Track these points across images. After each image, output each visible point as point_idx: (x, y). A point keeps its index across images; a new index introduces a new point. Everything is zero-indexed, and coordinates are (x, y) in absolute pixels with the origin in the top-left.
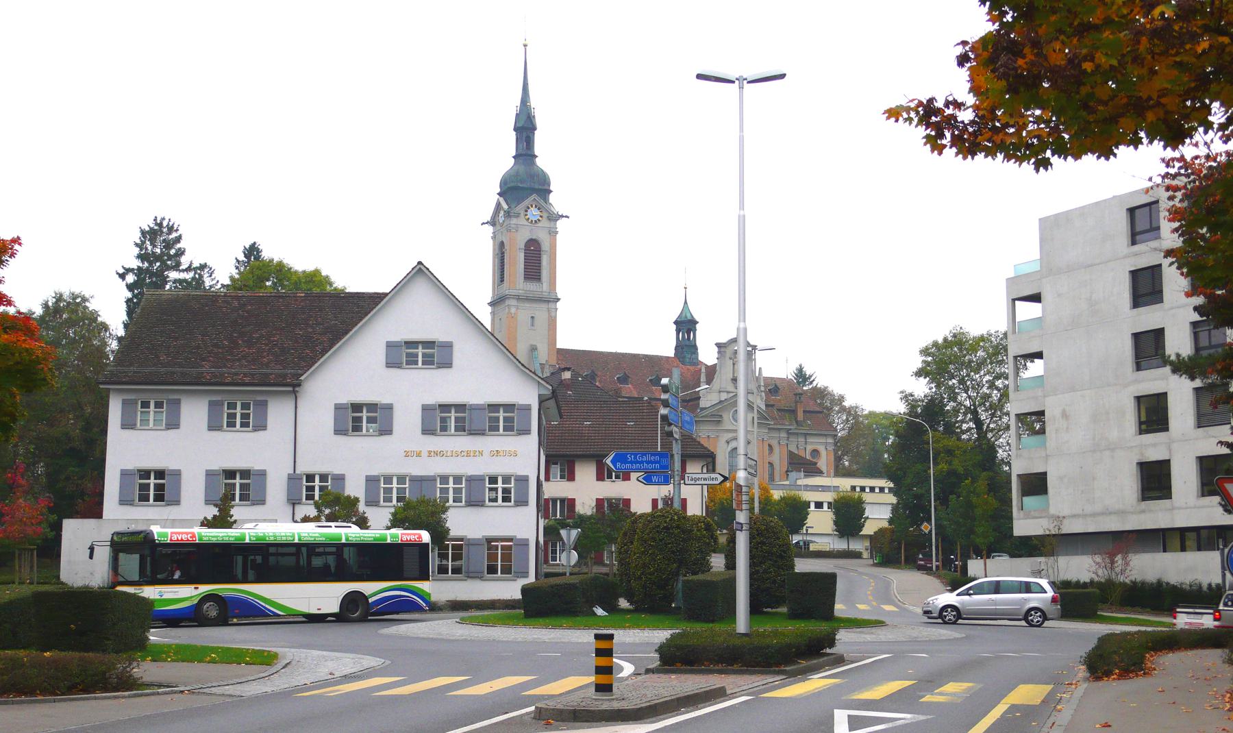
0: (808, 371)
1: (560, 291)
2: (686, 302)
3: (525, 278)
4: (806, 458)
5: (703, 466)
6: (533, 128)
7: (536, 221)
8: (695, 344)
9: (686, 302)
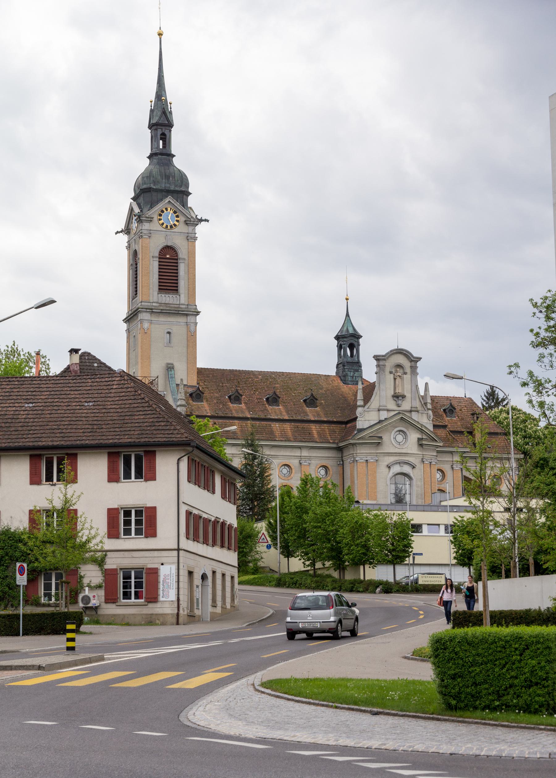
1: (200, 304)
2: (348, 315)
3: (159, 289)
5: (179, 460)
6: (170, 125)
8: (359, 360)
9: (348, 315)
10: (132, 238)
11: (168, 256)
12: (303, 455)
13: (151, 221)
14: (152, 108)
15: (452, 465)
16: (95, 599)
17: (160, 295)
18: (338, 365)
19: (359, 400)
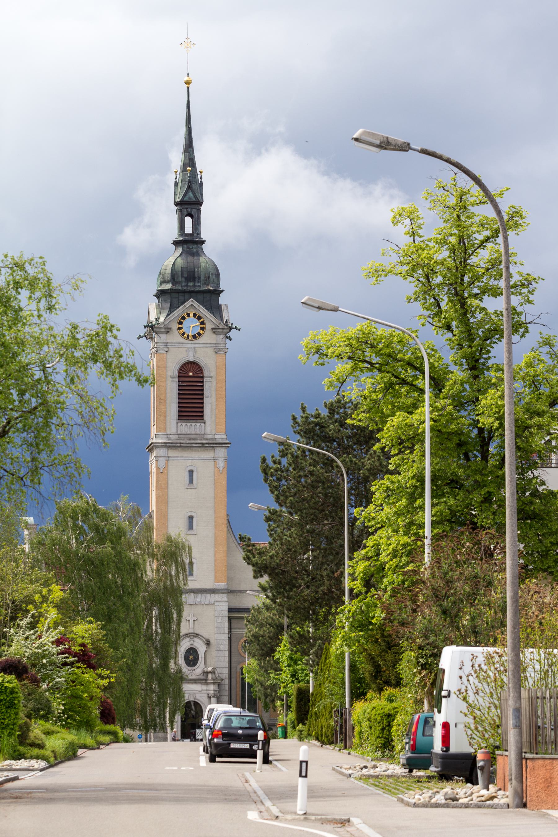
3: (179, 416)
11: (191, 374)
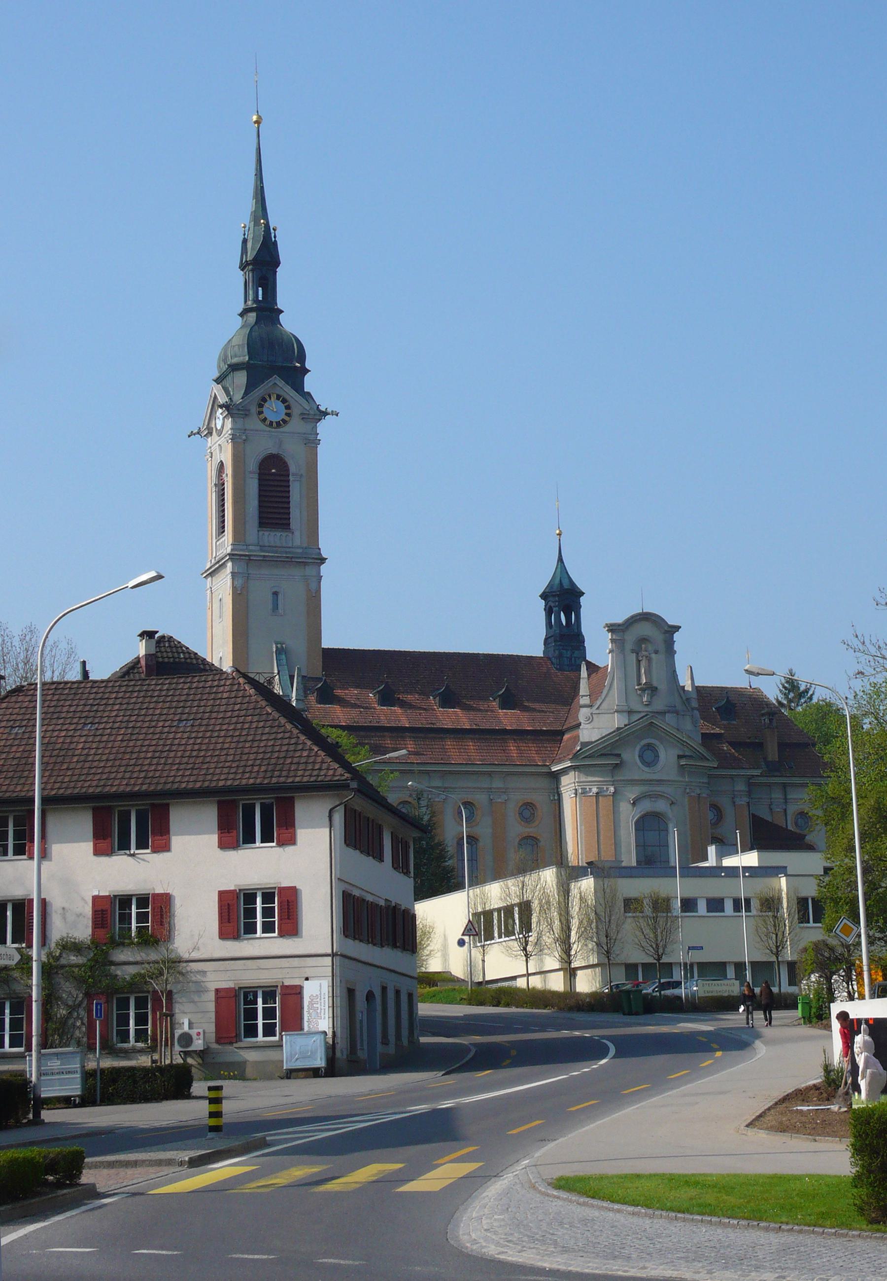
0: (803, 678)
1: (326, 546)
2: (560, 559)
3: (260, 523)
4: (786, 829)
7: (278, 424)
9: (560, 559)
10: (216, 443)
12: (494, 786)
13: (246, 415)
14: (246, 236)
15: (733, 798)
16: (199, 1039)
17: (262, 532)
18: (546, 640)
19: (583, 696)
